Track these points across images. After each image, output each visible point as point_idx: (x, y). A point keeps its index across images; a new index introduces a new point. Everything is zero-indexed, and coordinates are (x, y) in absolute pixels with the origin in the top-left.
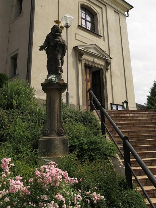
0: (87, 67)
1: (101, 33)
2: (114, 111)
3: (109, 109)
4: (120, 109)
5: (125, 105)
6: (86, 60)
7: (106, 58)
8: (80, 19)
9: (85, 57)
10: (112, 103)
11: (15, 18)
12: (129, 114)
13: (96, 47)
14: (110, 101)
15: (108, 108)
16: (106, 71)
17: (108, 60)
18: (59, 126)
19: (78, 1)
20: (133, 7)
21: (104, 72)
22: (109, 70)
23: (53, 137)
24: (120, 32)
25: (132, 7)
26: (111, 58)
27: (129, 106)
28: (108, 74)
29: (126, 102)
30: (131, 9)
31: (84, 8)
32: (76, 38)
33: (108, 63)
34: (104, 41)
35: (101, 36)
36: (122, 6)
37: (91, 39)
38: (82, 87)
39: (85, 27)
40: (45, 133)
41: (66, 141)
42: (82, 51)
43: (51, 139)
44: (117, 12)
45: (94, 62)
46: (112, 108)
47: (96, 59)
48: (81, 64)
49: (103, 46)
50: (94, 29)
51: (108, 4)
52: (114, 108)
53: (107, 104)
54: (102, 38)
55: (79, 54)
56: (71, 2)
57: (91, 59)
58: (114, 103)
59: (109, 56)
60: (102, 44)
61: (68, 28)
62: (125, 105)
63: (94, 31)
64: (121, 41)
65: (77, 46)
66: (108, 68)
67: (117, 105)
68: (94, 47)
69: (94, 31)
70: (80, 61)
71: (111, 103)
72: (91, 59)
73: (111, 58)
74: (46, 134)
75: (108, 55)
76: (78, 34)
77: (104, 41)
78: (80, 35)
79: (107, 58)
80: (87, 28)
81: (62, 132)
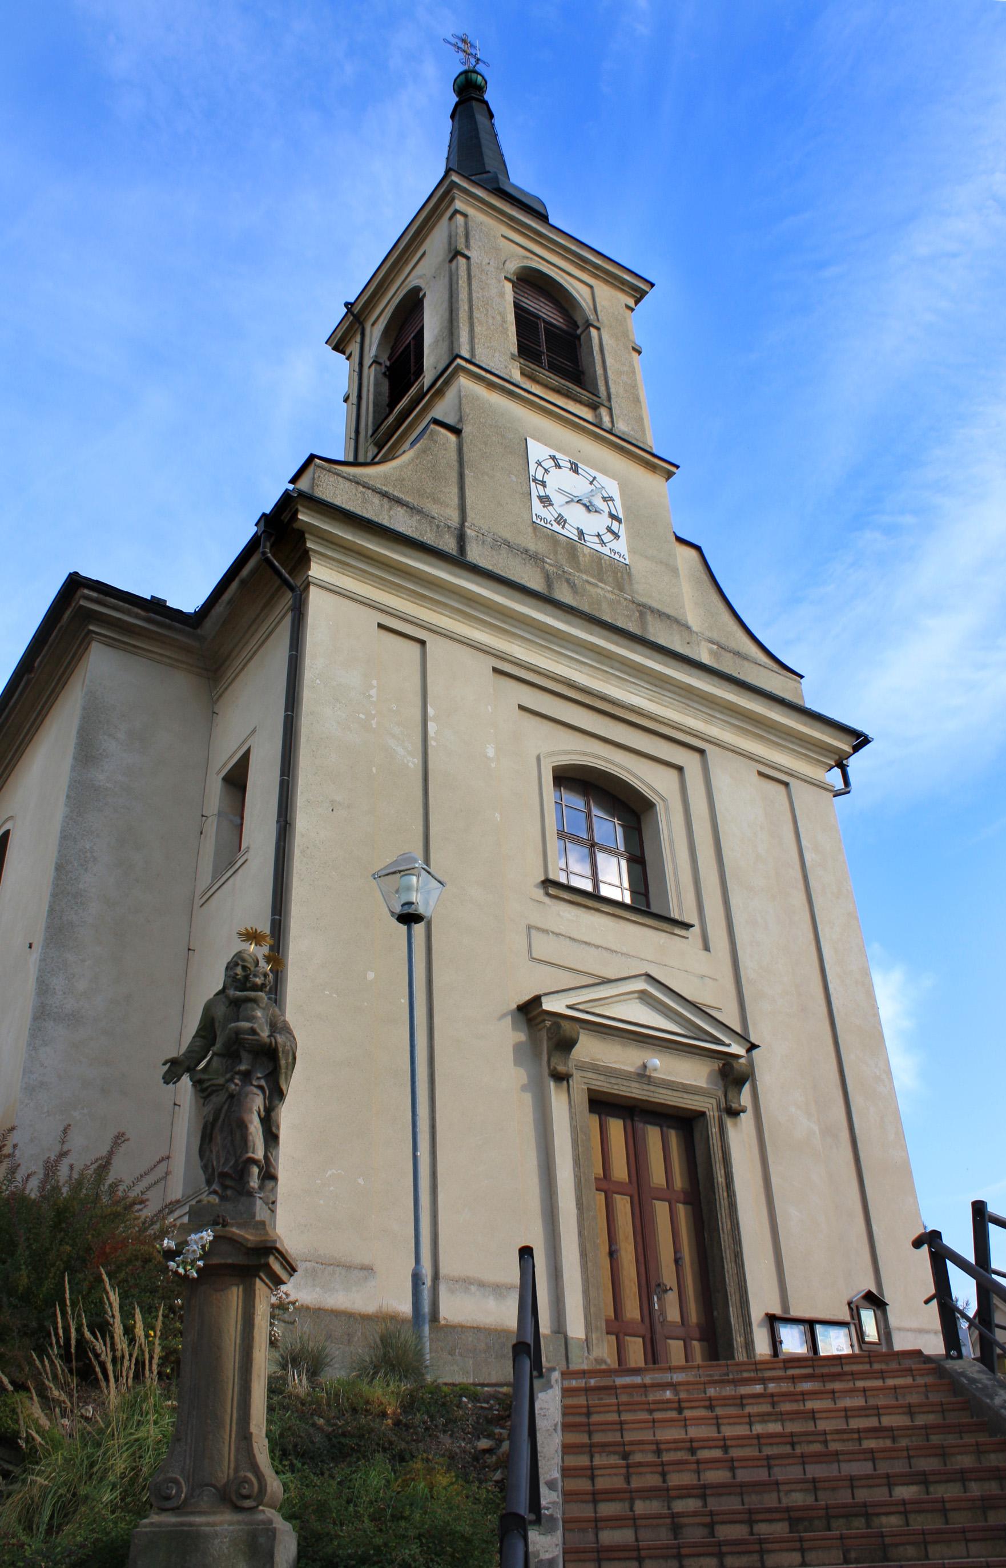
0: (602, 1104)
1: (680, 903)
2: (795, 1361)
3: (762, 1347)
4: (835, 1343)
5: (868, 1318)
6: (595, 1069)
7: (723, 1044)
8: (554, 843)
9: (588, 1049)
10: (777, 1311)
11: (215, 877)
12: (763, 1381)
13: (657, 991)
14: (762, 1300)
15: (749, 1345)
16: (729, 1123)
17: (737, 1057)
18: (237, 1460)
19: (536, 753)
20: (870, 735)
21: (714, 1130)
22: (746, 1119)
23: (198, 1519)
24: (801, 885)
25: (860, 740)
26: (753, 1047)
27: (893, 1321)
28: (740, 1138)
29: (875, 1301)
30: (856, 749)
31: (579, 780)
32: (534, 956)
33: (734, 1076)
34: (707, 948)
35: (687, 926)
36: (801, 740)
37: (624, 950)
38: (576, 1230)
39: (587, 886)
40: (168, 1498)
41: (262, 1540)
42: (566, 1025)
43: (191, 1525)
44: (772, 776)
45: (643, 1075)
46: (775, 1343)
47: (657, 1062)
48: (564, 1097)
49: (703, 977)
50: (643, 891)
51: (715, 744)
52: (793, 1342)
53: (747, 1324)
54: (696, 930)
55: (549, 1039)
56: (493, 765)
57: (625, 1058)
58: (794, 1313)
59: (743, 1037)
60: (690, 968)
61: (543, 879)
62: (868, 1318)
63: (648, 905)
64: (811, 936)
65: (537, 1000)
66: (734, 1106)
67: (810, 1325)
68: (643, 992)
69: (646, 904)
70: (561, 1078)
71: (771, 1312)
72: (625, 1058)
73: (753, 1047)
74: (168, 1504)
75: (739, 1030)
76: (546, 931)
77: (707, 948)
78: (557, 934)
79: (729, 1045)
80: (605, 891)
81: (244, 1492)
